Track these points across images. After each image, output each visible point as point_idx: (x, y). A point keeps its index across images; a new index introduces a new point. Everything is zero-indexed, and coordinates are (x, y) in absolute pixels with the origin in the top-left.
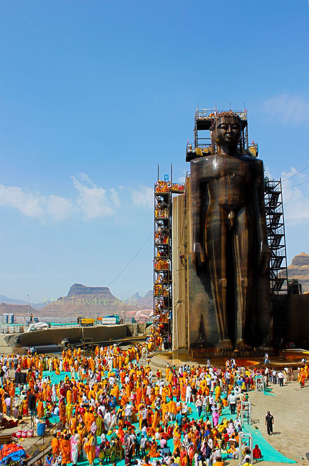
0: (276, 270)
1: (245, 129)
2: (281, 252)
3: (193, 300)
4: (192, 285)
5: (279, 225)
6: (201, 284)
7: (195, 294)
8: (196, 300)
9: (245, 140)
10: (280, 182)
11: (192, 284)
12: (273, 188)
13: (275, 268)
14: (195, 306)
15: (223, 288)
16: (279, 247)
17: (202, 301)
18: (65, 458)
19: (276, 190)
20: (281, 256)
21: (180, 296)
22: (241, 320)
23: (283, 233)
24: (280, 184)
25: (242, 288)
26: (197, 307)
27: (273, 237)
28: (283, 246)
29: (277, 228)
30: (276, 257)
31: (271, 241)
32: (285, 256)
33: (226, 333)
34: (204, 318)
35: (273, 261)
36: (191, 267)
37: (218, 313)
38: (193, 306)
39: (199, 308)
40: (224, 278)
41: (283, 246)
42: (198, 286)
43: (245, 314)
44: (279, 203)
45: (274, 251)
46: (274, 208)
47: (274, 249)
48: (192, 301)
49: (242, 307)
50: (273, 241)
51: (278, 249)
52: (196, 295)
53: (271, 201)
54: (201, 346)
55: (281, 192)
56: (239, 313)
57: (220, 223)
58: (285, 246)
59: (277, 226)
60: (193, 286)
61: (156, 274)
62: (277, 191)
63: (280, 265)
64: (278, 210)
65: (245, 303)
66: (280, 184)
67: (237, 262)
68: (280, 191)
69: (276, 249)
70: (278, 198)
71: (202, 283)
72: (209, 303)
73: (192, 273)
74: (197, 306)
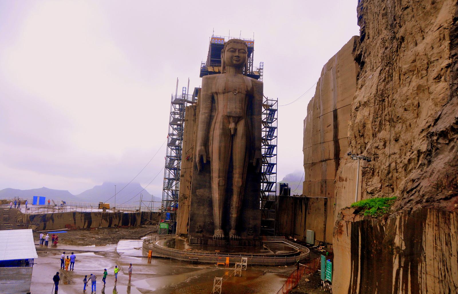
0: (268, 174)
1: (252, 54)
2: (273, 160)
5: (272, 155)
9: (251, 63)
10: (277, 101)
12: (271, 106)
13: (267, 173)
16: (272, 155)
18: (397, 111)
19: (274, 107)
20: (273, 163)
23: (276, 144)
24: (277, 103)
27: (268, 112)
28: (275, 155)
29: (272, 139)
30: (268, 163)
31: (266, 133)
32: (276, 163)
35: (266, 167)
41: (275, 155)
44: (273, 154)
45: (267, 176)
46: (271, 123)
47: (268, 157)
50: (268, 150)
51: (272, 157)
53: (269, 116)
55: (277, 110)
57: (228, 272)
58: (276, 173)
59: (272, 137)
62: (274, 108)
63: (272, 152)
64: (273, 142)
66: (277, 103)
68: (276, 109)
69: (270, 157)
70: (274, 114)
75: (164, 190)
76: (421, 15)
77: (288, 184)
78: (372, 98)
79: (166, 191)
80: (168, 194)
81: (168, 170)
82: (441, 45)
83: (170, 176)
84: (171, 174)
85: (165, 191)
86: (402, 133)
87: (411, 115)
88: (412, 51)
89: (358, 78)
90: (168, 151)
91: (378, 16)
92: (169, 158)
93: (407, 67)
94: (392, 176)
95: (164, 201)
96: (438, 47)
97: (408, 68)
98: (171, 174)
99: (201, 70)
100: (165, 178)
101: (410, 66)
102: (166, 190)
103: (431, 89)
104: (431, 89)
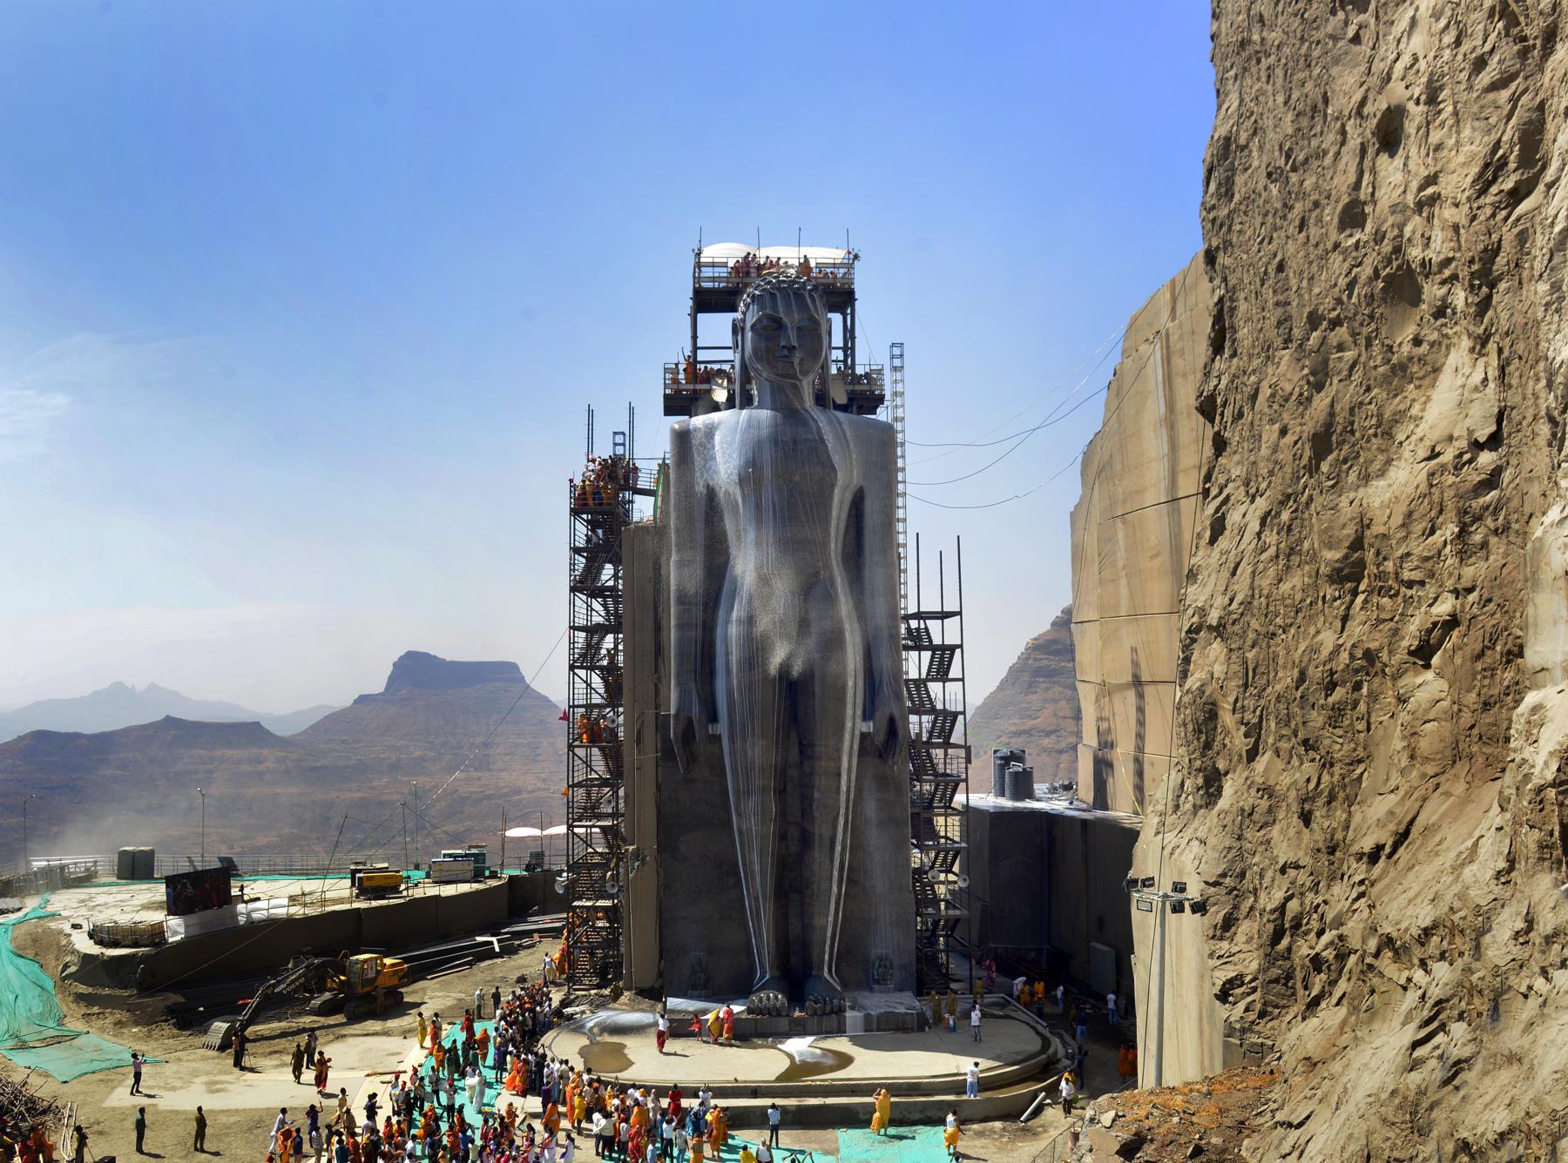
75: (572, 668)
76: (1381, 370)
77: (1024, 752)
78: (1235, 616)
79: (582, 673)
80: (589, 685)
81: (584, 597)
82: (1433, 526)
83: (593, 758)
84: (594, 613)
85: (574, 673)
86: (1317, 804)
87: (1345, 747)
88: (1351, 503)
89: (1207, 486)
90: (577, 538)
91: (1262, 285)
92: (583, 556)
93: (1337, 561)
94: (1289, 949)
95: (574, 706)
96: (1423, 534)
97: (1337, 565)
98: (594, 613)
99: (666, 397)
100: (573, 628)
101: (1346, 557)
102: (578, 668)
103: (1402, 687)
104: (1402, 687)
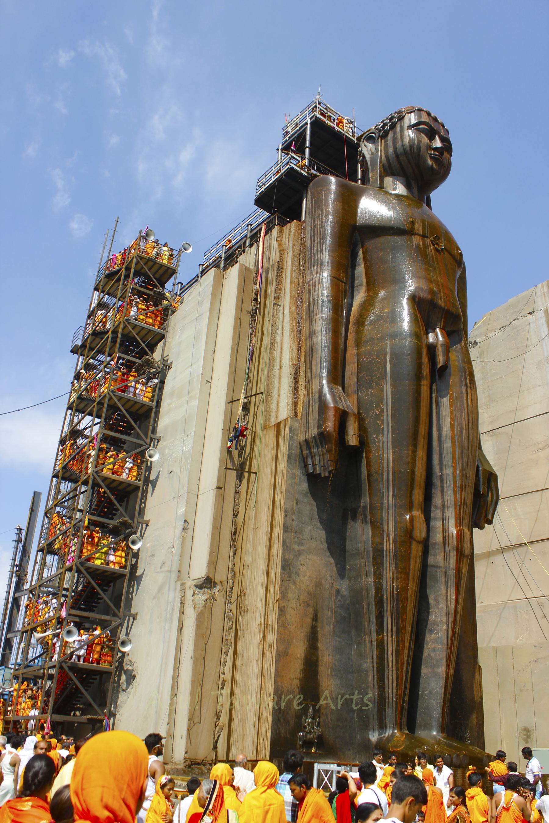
3: (293, 576)
4: (293, 520)
6: (319, 525)
7: (300, 553)
8: (302, 578)
11: (293, 517)
14: (298, 599)
15: (415, 540)
17: (318, 585)
21: (213, 563)
22: (444, 662)
25: (457, 555)
26: (304, 602)
33: (403, 706)
34: (321, 645)
36: (296, 460)
37: (380, 627)
38: (290, 595)
39: (308, 605)
40: (418, 510)
42: (310, 527)
43: (456, 643)
48: (290, 577)
49: (451, 619)
52: (301, 558)
54: (313, 750)
56: (435, 641)
60: (295, 523)
61: (46, 520)
65: (460, 607)
67: (441, 476)
71: (321, 523)
72: (336, 596)
73: (297, 480)
74: (302, 597)
